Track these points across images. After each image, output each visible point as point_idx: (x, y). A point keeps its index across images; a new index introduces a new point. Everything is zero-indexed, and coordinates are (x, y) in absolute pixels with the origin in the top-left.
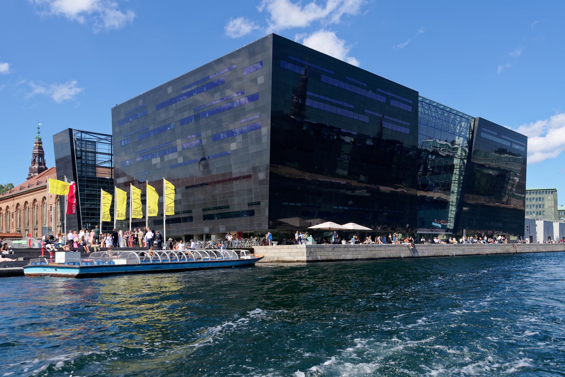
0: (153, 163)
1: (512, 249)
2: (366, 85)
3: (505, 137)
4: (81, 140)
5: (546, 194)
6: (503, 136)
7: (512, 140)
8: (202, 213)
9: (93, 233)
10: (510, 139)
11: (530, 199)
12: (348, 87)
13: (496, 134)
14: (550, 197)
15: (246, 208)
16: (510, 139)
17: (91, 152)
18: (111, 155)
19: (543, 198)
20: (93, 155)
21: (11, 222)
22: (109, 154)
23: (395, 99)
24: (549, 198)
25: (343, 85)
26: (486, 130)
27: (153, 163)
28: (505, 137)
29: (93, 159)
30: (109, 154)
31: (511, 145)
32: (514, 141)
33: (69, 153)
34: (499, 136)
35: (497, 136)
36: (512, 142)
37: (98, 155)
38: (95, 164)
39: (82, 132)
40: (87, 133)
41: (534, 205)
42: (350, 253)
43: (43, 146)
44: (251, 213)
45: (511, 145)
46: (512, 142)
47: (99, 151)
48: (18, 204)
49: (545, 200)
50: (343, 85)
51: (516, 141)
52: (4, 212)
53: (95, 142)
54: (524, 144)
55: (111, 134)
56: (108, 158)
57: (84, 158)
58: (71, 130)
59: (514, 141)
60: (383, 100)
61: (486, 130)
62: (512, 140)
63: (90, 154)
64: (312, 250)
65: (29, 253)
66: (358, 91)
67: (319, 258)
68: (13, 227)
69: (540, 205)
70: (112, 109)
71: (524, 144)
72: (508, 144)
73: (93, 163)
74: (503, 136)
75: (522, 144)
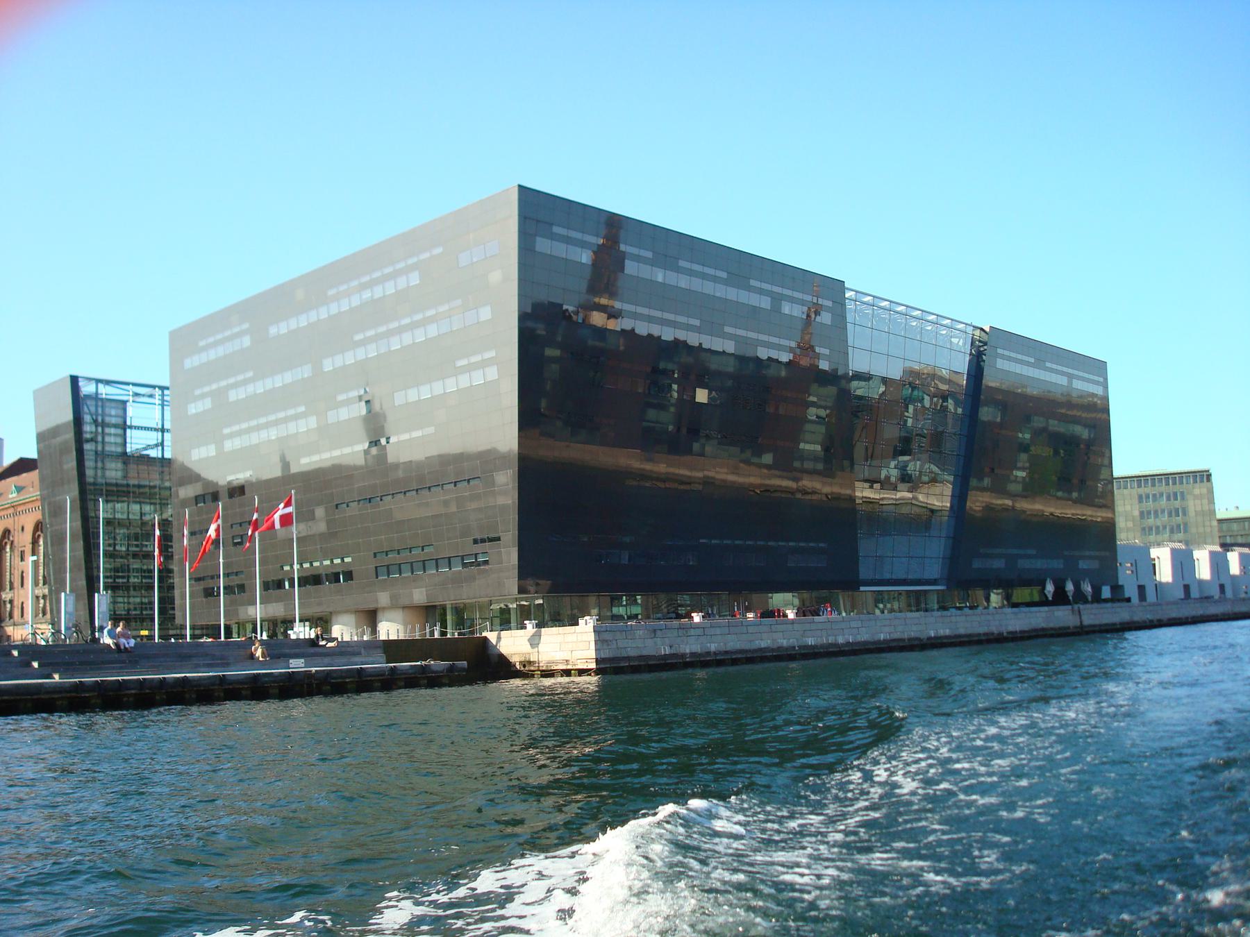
0: (231, 399)
3: (1054, 366)
4: (96, 397)
5: (1195, 482)
6: (1048, 364)
7: (1070, 371)
9: (894, 779)
10: (1065, 369)
11: (1154, 495)
12: (683, 282)
13: (1032, 360)
14: (1199, 489)
16: (1065, 369)
17: (115, 426)
18: (163, 430)
19: (1182, 493)
22: (156, 430)
23: (1079, 378)
24: (1197, 491)
25: (673, 278)
26: (1006, 353)
27: (231, 399)
28: (1054, 366)
30: (156, 430)
31: (1070, 382)
32: (1076, 372)
33: (68, 416)
34: (1039, 364)
36: (1071, 377)
39: (98, 381)
40: (108, 383)
41: (1149, 513)
42: (692, 640)
45: (1070, 382)
46: (1071, 377)
49: (1189, 497)
50: (673, 278)
51: (1081, 374)
53: (125, 402)
54: (1101, 380)
56: (154, 437)
57: (100, 438)
58: (74, 380)
59: (1076, 372)
60: (765, 303)
61: (1006, 353)
62: (1070, 371)
63: (113, 431)
66: (708, 288)
69: (1177, 511)
71: (1101, 380)
72: (1063, 381)
73: (119, 450)
74: (1048, 364)
75: (1096, 378)
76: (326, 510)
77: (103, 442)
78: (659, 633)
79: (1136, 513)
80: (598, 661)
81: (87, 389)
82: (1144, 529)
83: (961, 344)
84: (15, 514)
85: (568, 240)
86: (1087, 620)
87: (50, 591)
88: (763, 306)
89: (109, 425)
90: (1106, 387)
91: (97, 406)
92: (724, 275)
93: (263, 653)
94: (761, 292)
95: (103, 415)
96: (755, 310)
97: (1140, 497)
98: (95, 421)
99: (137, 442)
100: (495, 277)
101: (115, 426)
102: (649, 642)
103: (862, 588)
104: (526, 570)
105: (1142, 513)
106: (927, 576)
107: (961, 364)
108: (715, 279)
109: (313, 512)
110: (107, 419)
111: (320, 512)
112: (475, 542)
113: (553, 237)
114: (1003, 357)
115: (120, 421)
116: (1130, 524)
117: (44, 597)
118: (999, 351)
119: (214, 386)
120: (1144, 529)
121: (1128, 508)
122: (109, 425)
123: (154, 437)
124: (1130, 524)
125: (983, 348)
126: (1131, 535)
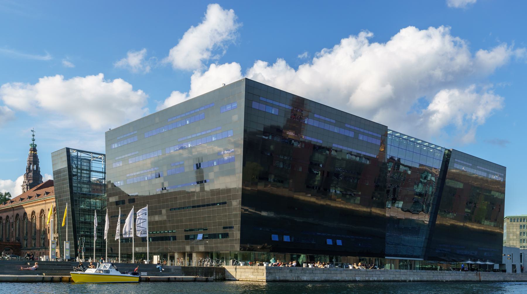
1: (475, 277)
2: (334, 121)
4: (77, 157)
8: (184, 234)
13: (471, 165)
15: (222, 231)
17: (86, 170)
20: (88, 172)
21: (11, 232)
22: (102, 172)
23: (363, 134)
26: (459, 161)
29: (88, 176)
33: (65, 165)
34: (474, 167)
35: (471, 167)
37: (93, 174)
38: (90, 181)
42: (307, 275)
43: (38, 153)
44: (225, 236)
46: (488, 173)
47: (93, 169)
48: (17, 215)
52: (4, 222)
53: (90, 160)
54: (503, 175)
55: (105, 153)
56: (101, 176)
58: (68, 150)
60: (351, 135)
64: (272, 271)
65: (55, 265)
66: (327, 127)
67: (278, 278)
68: (13, 236)
70: (106, 133)
72: (484, 175)
74: (478, 167)
76: (167, 211)
77: (81, 176)
78: (293, 271)
79: (518, 233)
80: (267, 281)
81: (74, 154)
82: (521, 240)
83: (440, 157)
84: (46, 203)
85: (266, 104)
86: (482, 279)
87: (59, 235)
88: (351, 135)
89: (84, 170)
90: (504, 177)
91: (77, 161)
92: (334, 121)
93: (321, 263)
94: (350, 130)
95: (81, 165)
96: (347, 137)
97: (521, 226)
98: (77, 168)
99: (95, 177)
100: (235, 118)
101: (86, 170)
102: (289, 275)
103: (386, 257)
104: (243, 241)
105: (521, 233)
106: (415, 254)
107: (437, 165)
108: (330, 123)
109: (161, 211)
110: (83, 167)
111: (164, 211)
112: (224, 228)
113: (260, 102)
114: (457, 163)
115: (88, 168)
116: (515, 237)
117: (57, 238)
118: (456, 160)
119: (123, 157)
120: (521, 240)
121: (515, 230)
122: (84, 170)
123: (101, 176)
124: (515, 237)
125: (448, 157)
126: (515, 242)
